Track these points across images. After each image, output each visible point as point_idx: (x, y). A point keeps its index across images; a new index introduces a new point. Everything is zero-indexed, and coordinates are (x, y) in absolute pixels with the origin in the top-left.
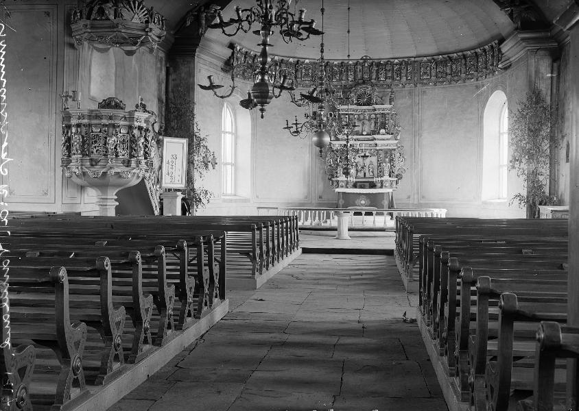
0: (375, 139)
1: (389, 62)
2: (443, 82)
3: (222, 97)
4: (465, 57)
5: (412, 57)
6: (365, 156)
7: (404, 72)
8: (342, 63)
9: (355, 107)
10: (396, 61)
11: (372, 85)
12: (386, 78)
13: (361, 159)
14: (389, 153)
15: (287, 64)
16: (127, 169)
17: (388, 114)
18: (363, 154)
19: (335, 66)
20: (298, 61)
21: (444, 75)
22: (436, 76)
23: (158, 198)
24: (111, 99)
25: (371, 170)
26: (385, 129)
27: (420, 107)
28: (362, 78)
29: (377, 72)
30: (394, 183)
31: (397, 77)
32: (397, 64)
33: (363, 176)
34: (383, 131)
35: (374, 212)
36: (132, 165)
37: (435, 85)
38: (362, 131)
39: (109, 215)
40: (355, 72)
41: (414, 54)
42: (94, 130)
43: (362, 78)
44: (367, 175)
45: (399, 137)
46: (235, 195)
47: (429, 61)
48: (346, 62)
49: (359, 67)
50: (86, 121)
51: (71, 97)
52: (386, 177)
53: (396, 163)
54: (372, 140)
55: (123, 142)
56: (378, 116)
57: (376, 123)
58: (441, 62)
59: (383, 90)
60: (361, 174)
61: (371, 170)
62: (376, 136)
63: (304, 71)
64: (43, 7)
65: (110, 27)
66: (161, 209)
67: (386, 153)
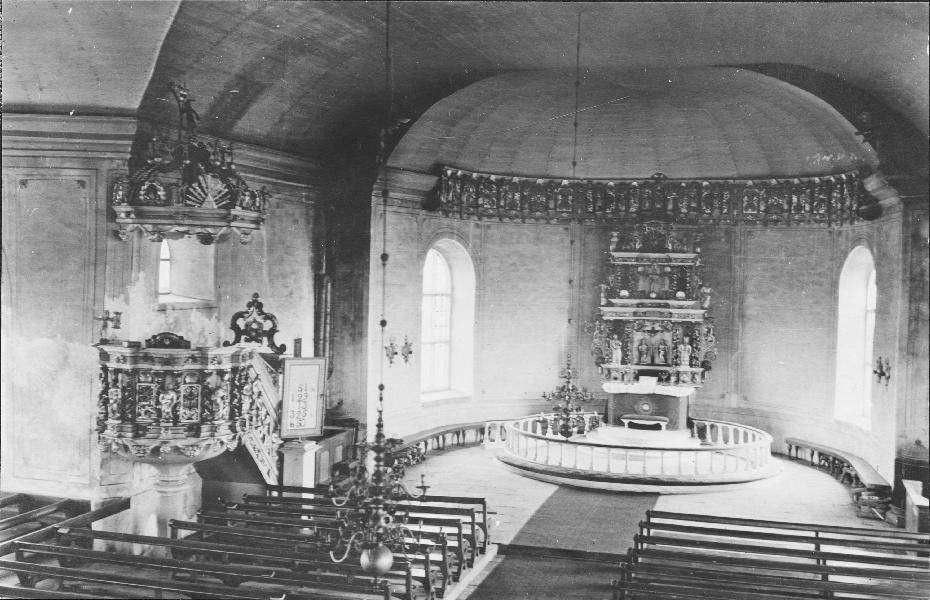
4: (811, 185)
5: (732, 178)
6: (653, 332)
13: (647, 336)
15: (536, 188)
16: (192, 441)
17: (690, 267)
19: (611, 188)
23: (275, 454)
24: (165, 336)
33: (649, 362)
34: (680, 294)
35: (663, 424)
36: (202, 434)
39: (139, 545)
41: (733, 173)
42: (142, 378)
44: (657, 361)
46: (449, 389)
47: (756, 185)
50: (127, 366)
51: (112, 320)
55: (190, 396)
60: (648, 360)
62: (671, 302)
63: (560, 197)
64: (77, 172)
65: (170, 217)
66: (281, 469)
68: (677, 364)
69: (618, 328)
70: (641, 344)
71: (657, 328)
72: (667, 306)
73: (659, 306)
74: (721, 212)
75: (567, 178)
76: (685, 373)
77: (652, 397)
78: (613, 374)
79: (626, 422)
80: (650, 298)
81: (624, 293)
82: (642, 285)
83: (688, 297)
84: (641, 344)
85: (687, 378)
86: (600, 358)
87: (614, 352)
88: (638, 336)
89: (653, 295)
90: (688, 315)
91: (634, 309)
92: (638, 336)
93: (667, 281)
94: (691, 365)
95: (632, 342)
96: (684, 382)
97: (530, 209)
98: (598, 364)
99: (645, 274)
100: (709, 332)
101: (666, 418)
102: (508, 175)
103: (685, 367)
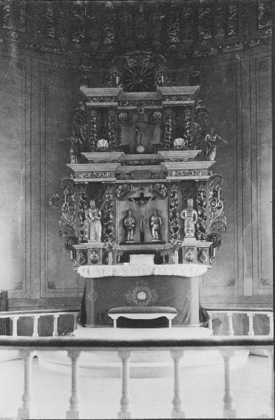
6: (142, 199)
13: (134, 205)
17: (189, 106)
25: (155, 226)
44: (148, 238)
60: (137, 238)
69: (95, 191)
70: (127, 217)
71: (147, 194)
72: (158, 162)
73: (149, 163)
74: (226, 33)
76: (191, 248)
77: (150, 280)
78: (91, 256)
79: (115, 317)
81: (103, 143)
84: (127, 217)
86: (70, 238)
88: (122, 206)
89: (141, 149)
90: (190, 172)
91: (114, 166)
92: (122, 206)
93: (158, 131)
95: (114, 214)
98: (69, 247)
100: (215, 196)
101: (174, 309)
103: (190, 241)
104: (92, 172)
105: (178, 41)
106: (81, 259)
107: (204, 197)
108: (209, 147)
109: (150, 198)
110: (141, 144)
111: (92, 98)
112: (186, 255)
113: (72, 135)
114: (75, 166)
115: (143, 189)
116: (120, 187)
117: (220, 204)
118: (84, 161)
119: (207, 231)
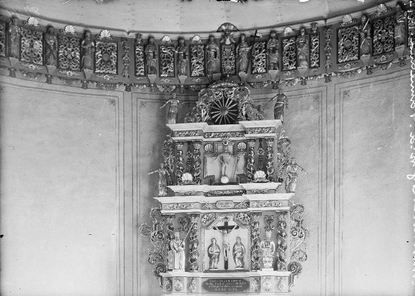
0: (245, 192)
1: (274, 34)
2: (387, 64)
3: (306, 256)
6: (226, 228)
7: (303, 50)
8: (180, 39)
9: (203, 126)
10: (289, 30)
11: (242, 83)
12: (267, 68)
13: (218, 234)
14: (274, 220)
18: (222, 224)
19: (166, 45)
20: (85, 32)
21: (389, 48)
22: (372, 52)
25: (239, 255)
26: (265, 170)
27: (337, 125)
28: (221, 69)
29: (250, 56)
30: (285, 283)
31: (290, 63)
32: (289, 38)
34: (260, 174)
37: (370, 71)
38: (221, 176)
40: (206, 58)
41: (324, 11)
43: (221, 69)
44: (232, 266)
45: (294, 187)
48: (187, 37)
49: (214, 48)
52: (267, 271)
53: (289, 241)
54: (240, 194)
56: (252, 144)
57: (247, 158)
58: (383, 19)
59: (263, 96)
60: (220, 266)
61: (239, 255)
62: (246, 186)
63: (99, 54)
67: (269, 221)
68: (257, 269)
74: (310, 64)
75: (108, 29)
80: (221, 184)
82: (212, 167)
83: (270, 179)
85: (183, 285)
87: (177, 255)
94: (275, 268)
96: (267, 290)
97: (58, 66)
99: (214, 153)
102: (24, 13)
104: (178, 204)
105: (264, 71)
106: (168, 287)
107: (285, 227)
108: (290, 178)
109: (233, 227)
110: (225, 175)
111: (178, 132)
112: (264, 284)
113: (160, 168)
114: (164, 200)
115: (226, 218)
116: (205, 217)
117: (301, 233)
118: (170, 193)
119: (286, 260)
